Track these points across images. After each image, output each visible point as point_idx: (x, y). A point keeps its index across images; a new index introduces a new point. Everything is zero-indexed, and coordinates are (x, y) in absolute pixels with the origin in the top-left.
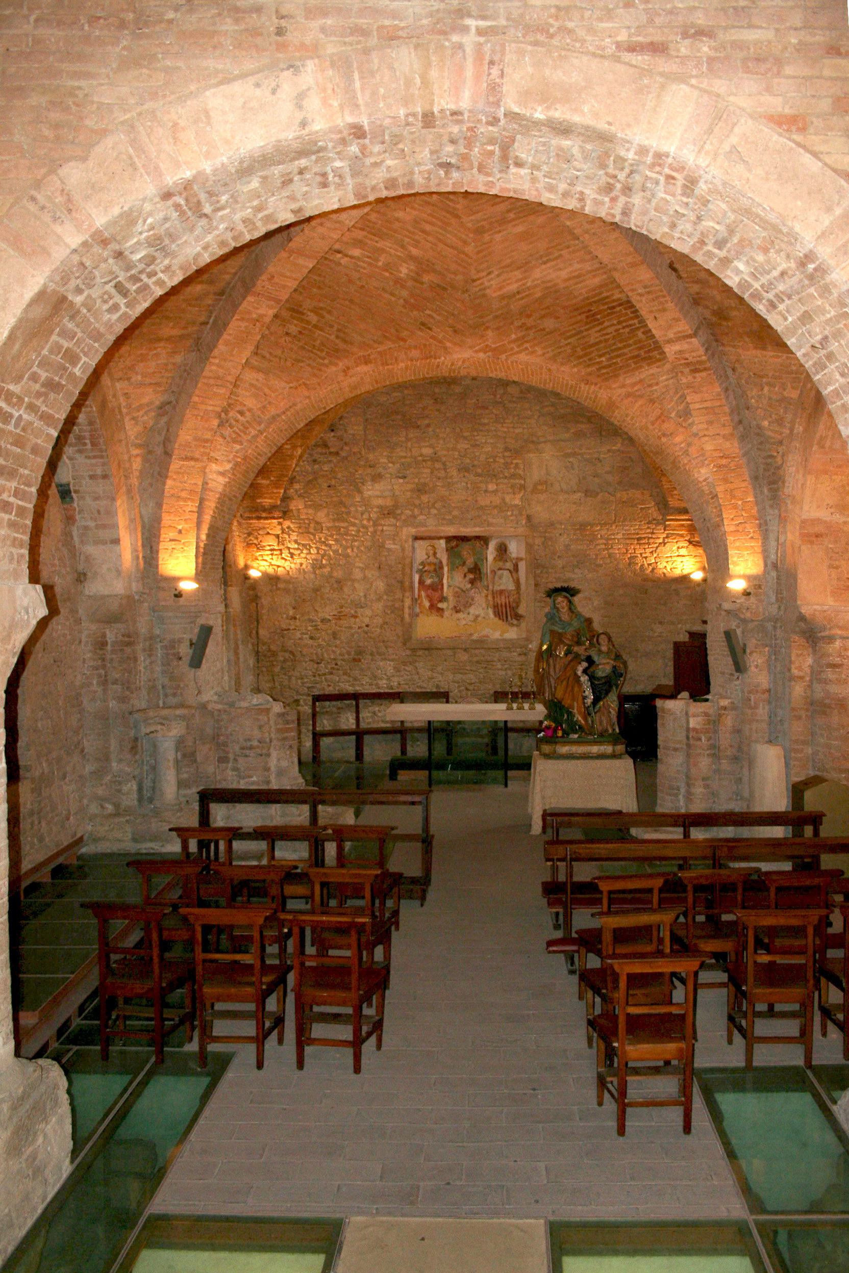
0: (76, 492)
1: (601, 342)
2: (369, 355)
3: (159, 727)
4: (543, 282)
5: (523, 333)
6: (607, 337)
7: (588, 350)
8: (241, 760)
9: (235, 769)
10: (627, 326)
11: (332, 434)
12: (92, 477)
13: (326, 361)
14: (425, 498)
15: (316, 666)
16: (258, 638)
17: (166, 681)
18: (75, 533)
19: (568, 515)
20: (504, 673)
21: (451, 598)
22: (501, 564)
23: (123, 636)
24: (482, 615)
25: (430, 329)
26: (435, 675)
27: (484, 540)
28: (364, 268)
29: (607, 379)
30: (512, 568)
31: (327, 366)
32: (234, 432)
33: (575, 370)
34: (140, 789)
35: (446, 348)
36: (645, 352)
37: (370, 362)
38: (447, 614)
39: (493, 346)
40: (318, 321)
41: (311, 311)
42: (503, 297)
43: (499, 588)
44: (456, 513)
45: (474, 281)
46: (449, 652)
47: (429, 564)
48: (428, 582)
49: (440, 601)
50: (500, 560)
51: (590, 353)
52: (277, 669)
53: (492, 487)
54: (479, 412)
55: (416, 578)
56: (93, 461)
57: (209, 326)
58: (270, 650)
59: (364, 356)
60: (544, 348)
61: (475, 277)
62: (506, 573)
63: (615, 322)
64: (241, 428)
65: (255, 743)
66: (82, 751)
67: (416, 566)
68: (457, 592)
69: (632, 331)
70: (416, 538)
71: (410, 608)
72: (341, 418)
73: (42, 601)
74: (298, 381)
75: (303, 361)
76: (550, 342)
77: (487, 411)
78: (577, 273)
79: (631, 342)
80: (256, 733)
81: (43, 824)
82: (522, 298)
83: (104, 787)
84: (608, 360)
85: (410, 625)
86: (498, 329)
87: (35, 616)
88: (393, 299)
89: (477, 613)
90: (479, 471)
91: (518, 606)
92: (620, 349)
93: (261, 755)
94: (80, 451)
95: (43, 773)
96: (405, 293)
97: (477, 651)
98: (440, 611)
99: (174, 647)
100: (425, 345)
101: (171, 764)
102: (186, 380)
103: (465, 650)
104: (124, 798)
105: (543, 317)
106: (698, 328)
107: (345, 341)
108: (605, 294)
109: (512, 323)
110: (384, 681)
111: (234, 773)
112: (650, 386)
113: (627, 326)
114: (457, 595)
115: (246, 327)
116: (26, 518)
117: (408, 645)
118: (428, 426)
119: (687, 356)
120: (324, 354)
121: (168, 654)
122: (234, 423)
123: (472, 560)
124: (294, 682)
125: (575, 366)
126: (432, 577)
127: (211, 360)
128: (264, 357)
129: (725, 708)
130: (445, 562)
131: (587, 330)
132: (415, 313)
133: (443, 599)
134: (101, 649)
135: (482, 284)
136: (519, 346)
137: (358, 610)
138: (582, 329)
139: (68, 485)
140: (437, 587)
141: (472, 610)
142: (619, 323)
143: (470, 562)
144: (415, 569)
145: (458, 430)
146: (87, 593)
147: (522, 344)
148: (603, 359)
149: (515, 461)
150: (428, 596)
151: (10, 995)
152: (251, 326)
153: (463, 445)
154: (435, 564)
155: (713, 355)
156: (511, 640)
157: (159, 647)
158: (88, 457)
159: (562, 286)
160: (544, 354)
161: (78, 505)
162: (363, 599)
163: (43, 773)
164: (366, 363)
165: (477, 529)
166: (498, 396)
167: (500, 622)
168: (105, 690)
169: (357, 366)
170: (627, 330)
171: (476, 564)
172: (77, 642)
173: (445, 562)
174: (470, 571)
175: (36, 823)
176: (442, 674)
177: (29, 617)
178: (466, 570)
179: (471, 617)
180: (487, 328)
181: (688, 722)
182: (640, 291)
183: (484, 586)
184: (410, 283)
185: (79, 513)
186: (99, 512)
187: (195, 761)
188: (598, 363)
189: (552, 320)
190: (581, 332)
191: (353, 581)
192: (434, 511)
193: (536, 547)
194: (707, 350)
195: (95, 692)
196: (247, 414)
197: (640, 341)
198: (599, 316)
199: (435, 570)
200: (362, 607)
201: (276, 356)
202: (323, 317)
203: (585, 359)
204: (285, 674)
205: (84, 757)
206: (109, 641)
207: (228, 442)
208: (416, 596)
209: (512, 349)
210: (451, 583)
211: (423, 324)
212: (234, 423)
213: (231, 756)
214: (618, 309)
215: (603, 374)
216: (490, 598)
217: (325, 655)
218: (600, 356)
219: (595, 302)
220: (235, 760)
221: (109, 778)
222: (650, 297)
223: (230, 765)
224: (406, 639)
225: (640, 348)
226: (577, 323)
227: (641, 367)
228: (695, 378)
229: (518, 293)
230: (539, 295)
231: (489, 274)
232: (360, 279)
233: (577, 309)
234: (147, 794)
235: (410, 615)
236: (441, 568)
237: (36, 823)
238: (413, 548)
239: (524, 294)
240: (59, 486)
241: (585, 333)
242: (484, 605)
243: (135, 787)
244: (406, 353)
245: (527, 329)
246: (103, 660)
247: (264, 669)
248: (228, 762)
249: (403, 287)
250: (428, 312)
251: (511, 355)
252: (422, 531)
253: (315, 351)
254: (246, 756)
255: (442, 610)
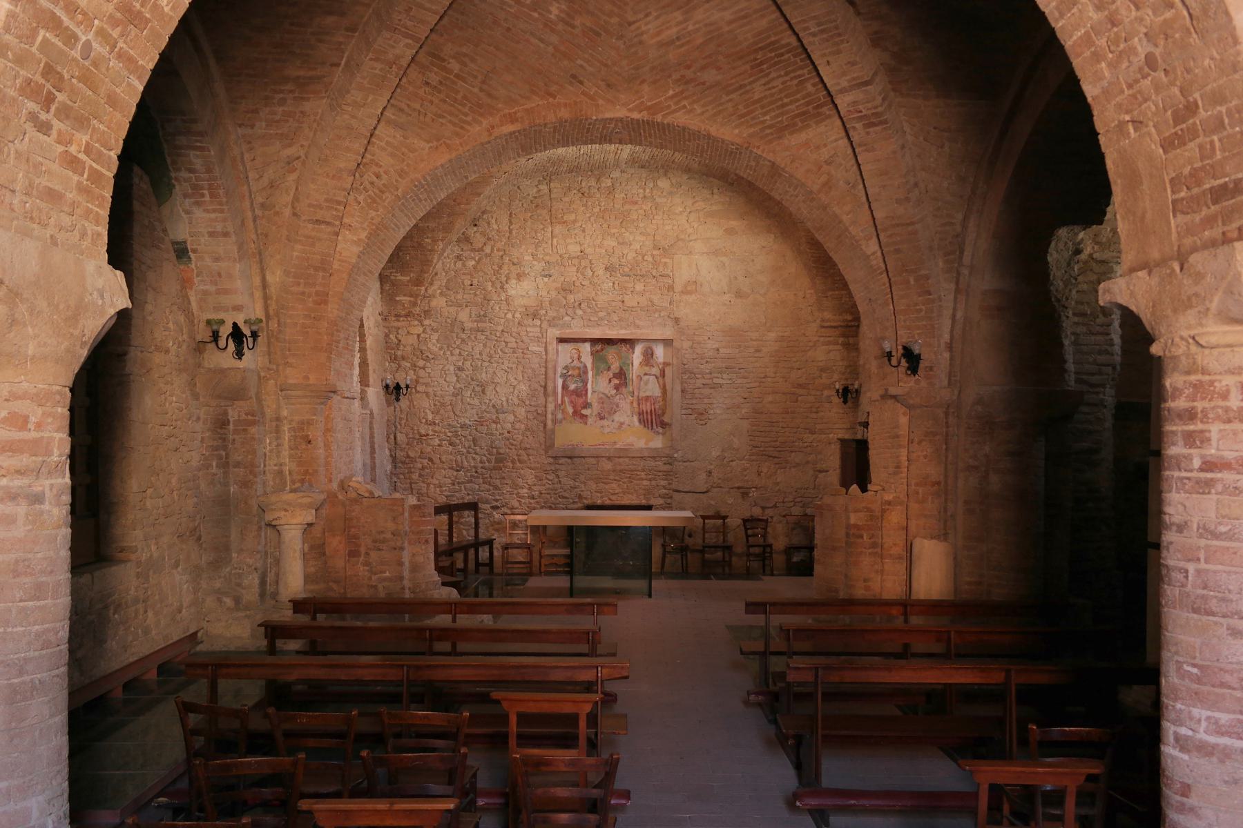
0: (194, 251)
1: (765, 97)
2: (515, 113)
3: (283, 513)
4: (706, 25)
5: (681, 89)
6: (774, 91)
7: (751, 108)
8: (374, 555)
9: (367, 564)
10: (796, 77)
11: (475, 229)
12: (211, 234)
13: (469, 119)
14: (571, 298)
15: (455, 473)
16: (396, 443)
17: (294, 466)
18: (193, 299)
19: (718, 317)
20: (648, 483)
21: (595, 405)
22: (647, 369)
23: (246, 414)
24: (627, 422)
25: (581, 83)
26: (577, 484)
27: (630, 343)
28: (510, 6)
29: (771, 142)
30: (658, 374)
31: (469, 124)
32: (369, 196)
33: (737, 131)
34: (263, 583)
35: (597, 106)
36: (815, 108)
37: (517, 120)
38: (590, 420)
39: (649, 104)
40: (460, 70)
41: (454, 58)
42: (661, 45)
43: (644, 395)
44: (601, 314)
45: (630, 24)
46: (593, 461)
47: (574, 368)
48: (572, 387)
49: (585, 407)
50: (646, 365)
51: (752, 111)
52: (415, 476)
53: (639, 287)
54: (627, 207)
55: (560, 382)
56: (213, 216)
57: (340, 68)
58: (408, 456)
59: (509, 114)
60: (703, 106)
61: (631, 19)
62: (652, 378)
63: (782, 73)
64: (377, 192)
65: (389, 536)
66: (199, 539)
67: (559, 370)
68: (601, 398)
69: (801, 83)
70: (562, 340)
71: (552, 414)
72: (483, 213)
73: (122, 289)
74: (438, 140)
75: (444, 117)
76: (710, 99)
77: (636, 207)
78: (743, 13)
79: (798, 96)
80: (391, 526)
81: (150, 614)
82: (682, 45)
83: (223, 579)
84: (772, 118)
85: (553, 431)
86: (654, 82)
87: (112, 305)
88: (542, 45)
89: (622, 420)
90: (626, 270)
91: (664, 413)
92: (787, 104)
93: (395, 549)
94: (198, 204)
95: (151, 556)
96: (554, 39)
97: (621, 460)
98: (584, 417)
99: (303, 429)
100: (576, 103)
101: (298, 554)
102: (316, 131)
103: (609, 458)
104: (244, 592)
105: (703, 68)
106: (875, 74)
107: (490, 95)
108: (773, 39)
109: (670, 76)
110: (525, 491)
111: (367, 568)
112: (818, 148)
113: (796, 77)
114: (601, 401)
115: (381, 70)
116: (103, 188)
117: (550, 453)
118: (574, 222)
119: (861, 107)
120: (466, 110)
121: (296, 437)
122: (369, 186)
123: (618, 365)
124: (433, 490)
125: (736, 127)
126: (576, 382)
127: (344, 107)
128: (401, 110)
129: (889, 503)
130: (589, 366)
131: (750, 83)
132: (566, 62)
133: (587, 405)
134: (221, 428)
135: (639, 28)
136: (676, 104)
137: (500, 415)
138: (746, 82)
139: (185, 242)
140: (581, 393)
141: (617, 417)
142: (787, 74)
143: (615, 367)
144: (558, 375)
145: (605, 226)
146: (206, 365)
147: (679, 101)
148: (768, 117)
149: (663, 260)
150: (572, 402)
151: (66, 770)
152: (388, 68)
153: (611, 243)
154: (579, 368)
155: (890, 106)
156: (655, 449)
157: (286, 429)
158: (208, 211)
159: (726, 29)
160: (703, 113)
161: (197, 268)
162: (505, 403)
163: (151, 556)
164: (512, 122)
165: (623, 332)
166: (648, 191)
167: (646, 430)
168: (226, 474)
169: (502, 125)
170: (795, 82)
171: (621, 369)
172: (194, 418)
173: (589, 366)
174: (615, 376)
175: (141, 611)
176: (584, 483)
177: (104, 303)
178: (611, 375)
179: (616, 425)
180: (643, 81)
181: (848, 518)
182: (813, 30)
183: (630, 392)
184: (560, 27)
185: (197, 276)
186: (220, 275)
187: (324, 554)
188: (763, 122)
189: (714, 72)
190: (745, 85)
191: (497, 384)
192: (579, 312)
193: (684, 351)
194: (884, 99)
195: (215, 475)
196: (385, 176)
197: (809, 95)
198: (765, 66)
199: (579, 375)
200: (504, 413)
201: (414, 109)
202: (466, 65)
203: (748, 118)
204: (423, 482)
205: (200, 546)
206: (231, 420)
207: (362, 208)
208: (560, 402)
209: (669, 106)
210: (596, 389)
211: (574, 76)
212: (369, 186)
213: (363, 550)
214: (786, 56)
215: (767, 135)
216: (635, 405)
217: (465, 463)
218: (765, 114)
219: (761, 49)
220: (367, 554)
221: (228, 570)
222: (825, 36)
223: (362, 559)
224: (549, 446)
225: (808, 104)
226: (740, 75)
227: (808, 126)
228: (868, 133)
229: (678, 38)
230: (700, 41)
231: (647, 15)
232: (506, 20)
233: (741, 58)
234: (270, 589)
235: (552, 421)
236: (586, 372)
237: (141, 611)
238: (557, 351)
239: (683, 41)
240: (174, 243)
241: (748, 88)
242: (629, 413)
243: (257, 581)
244: (555, 112)
245: (686, 83)
246: (224, 440)
247: (402, 476)
248: (360, 556)
249: (553, 31)
250: (579, 62)
251: (668, 114)
252: (568, 333)
253: (456, 105)
254: (379, 550)
255: (586, 416)
